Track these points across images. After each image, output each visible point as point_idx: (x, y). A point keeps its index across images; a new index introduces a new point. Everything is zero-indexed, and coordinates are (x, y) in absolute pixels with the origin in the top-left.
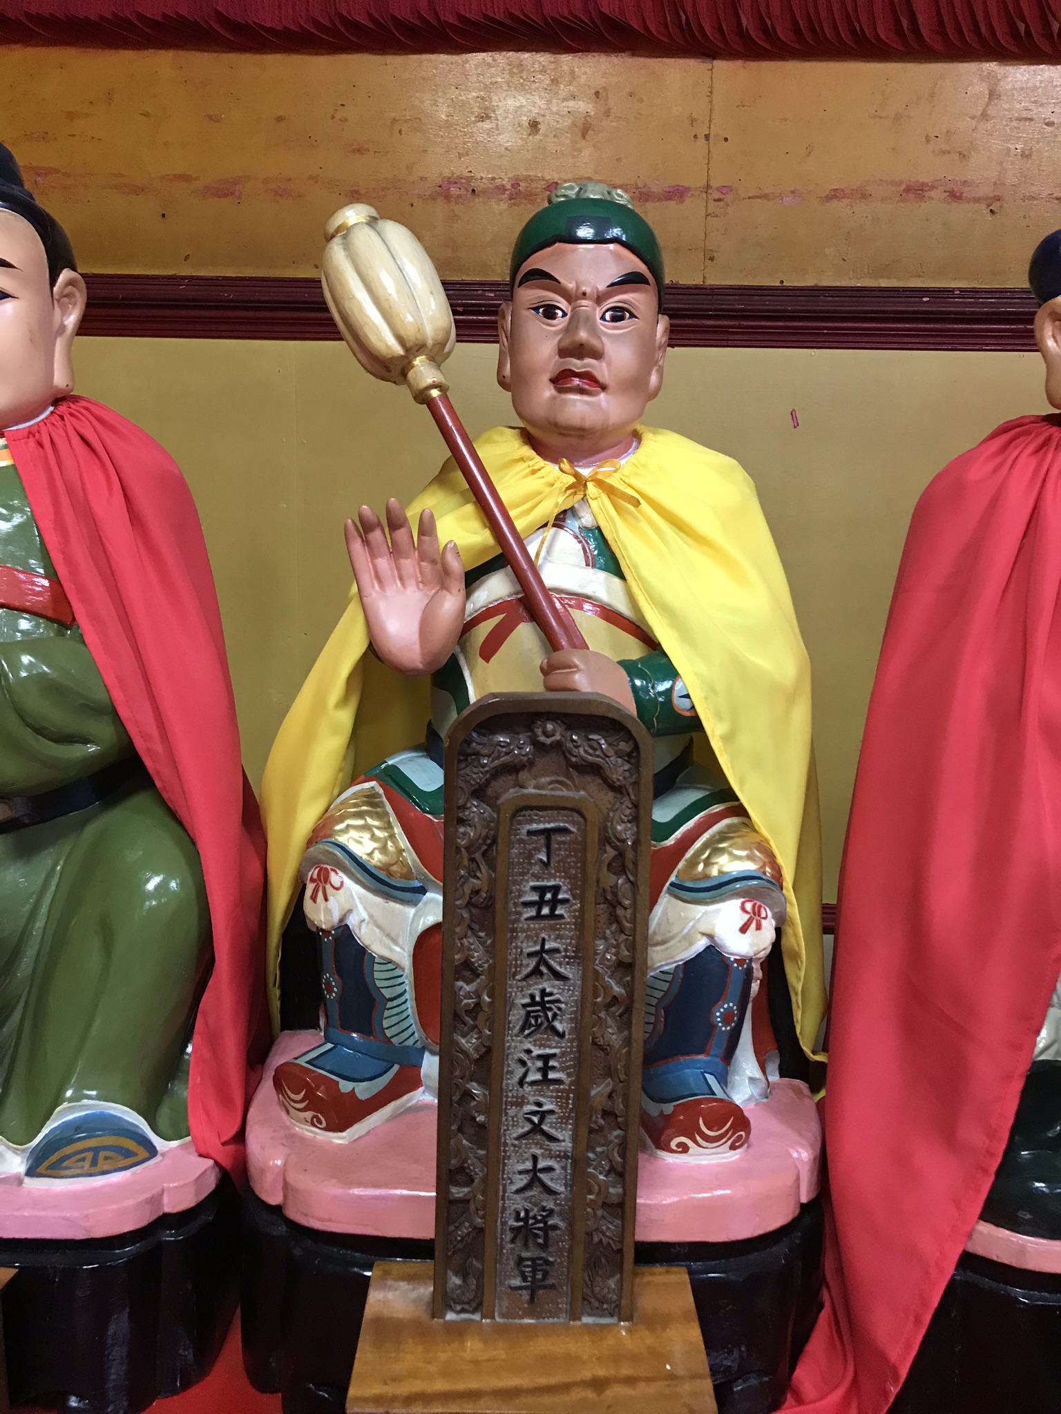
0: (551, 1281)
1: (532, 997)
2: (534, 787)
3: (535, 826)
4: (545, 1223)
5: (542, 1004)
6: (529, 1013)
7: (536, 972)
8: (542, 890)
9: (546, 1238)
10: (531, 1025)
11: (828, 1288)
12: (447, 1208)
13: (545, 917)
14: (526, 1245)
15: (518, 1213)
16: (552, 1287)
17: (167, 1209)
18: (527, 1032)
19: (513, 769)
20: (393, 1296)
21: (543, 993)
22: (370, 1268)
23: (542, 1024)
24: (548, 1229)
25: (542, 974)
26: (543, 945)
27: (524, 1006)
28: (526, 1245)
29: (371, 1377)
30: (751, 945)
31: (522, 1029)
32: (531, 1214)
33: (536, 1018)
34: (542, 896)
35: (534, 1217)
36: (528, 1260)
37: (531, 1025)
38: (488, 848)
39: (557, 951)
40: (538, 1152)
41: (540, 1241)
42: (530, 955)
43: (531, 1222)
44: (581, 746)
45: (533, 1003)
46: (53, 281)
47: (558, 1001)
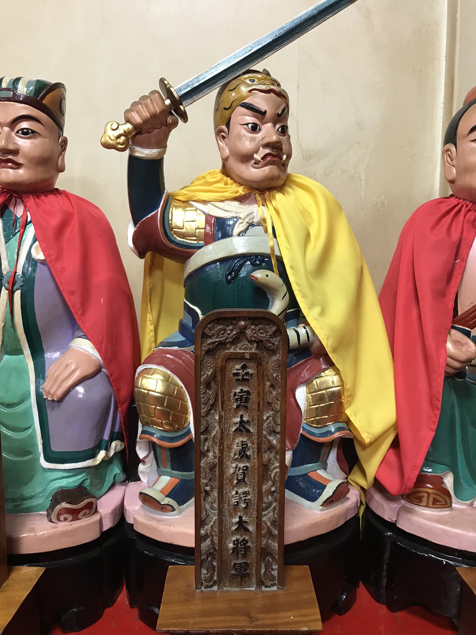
11: (240, 199)
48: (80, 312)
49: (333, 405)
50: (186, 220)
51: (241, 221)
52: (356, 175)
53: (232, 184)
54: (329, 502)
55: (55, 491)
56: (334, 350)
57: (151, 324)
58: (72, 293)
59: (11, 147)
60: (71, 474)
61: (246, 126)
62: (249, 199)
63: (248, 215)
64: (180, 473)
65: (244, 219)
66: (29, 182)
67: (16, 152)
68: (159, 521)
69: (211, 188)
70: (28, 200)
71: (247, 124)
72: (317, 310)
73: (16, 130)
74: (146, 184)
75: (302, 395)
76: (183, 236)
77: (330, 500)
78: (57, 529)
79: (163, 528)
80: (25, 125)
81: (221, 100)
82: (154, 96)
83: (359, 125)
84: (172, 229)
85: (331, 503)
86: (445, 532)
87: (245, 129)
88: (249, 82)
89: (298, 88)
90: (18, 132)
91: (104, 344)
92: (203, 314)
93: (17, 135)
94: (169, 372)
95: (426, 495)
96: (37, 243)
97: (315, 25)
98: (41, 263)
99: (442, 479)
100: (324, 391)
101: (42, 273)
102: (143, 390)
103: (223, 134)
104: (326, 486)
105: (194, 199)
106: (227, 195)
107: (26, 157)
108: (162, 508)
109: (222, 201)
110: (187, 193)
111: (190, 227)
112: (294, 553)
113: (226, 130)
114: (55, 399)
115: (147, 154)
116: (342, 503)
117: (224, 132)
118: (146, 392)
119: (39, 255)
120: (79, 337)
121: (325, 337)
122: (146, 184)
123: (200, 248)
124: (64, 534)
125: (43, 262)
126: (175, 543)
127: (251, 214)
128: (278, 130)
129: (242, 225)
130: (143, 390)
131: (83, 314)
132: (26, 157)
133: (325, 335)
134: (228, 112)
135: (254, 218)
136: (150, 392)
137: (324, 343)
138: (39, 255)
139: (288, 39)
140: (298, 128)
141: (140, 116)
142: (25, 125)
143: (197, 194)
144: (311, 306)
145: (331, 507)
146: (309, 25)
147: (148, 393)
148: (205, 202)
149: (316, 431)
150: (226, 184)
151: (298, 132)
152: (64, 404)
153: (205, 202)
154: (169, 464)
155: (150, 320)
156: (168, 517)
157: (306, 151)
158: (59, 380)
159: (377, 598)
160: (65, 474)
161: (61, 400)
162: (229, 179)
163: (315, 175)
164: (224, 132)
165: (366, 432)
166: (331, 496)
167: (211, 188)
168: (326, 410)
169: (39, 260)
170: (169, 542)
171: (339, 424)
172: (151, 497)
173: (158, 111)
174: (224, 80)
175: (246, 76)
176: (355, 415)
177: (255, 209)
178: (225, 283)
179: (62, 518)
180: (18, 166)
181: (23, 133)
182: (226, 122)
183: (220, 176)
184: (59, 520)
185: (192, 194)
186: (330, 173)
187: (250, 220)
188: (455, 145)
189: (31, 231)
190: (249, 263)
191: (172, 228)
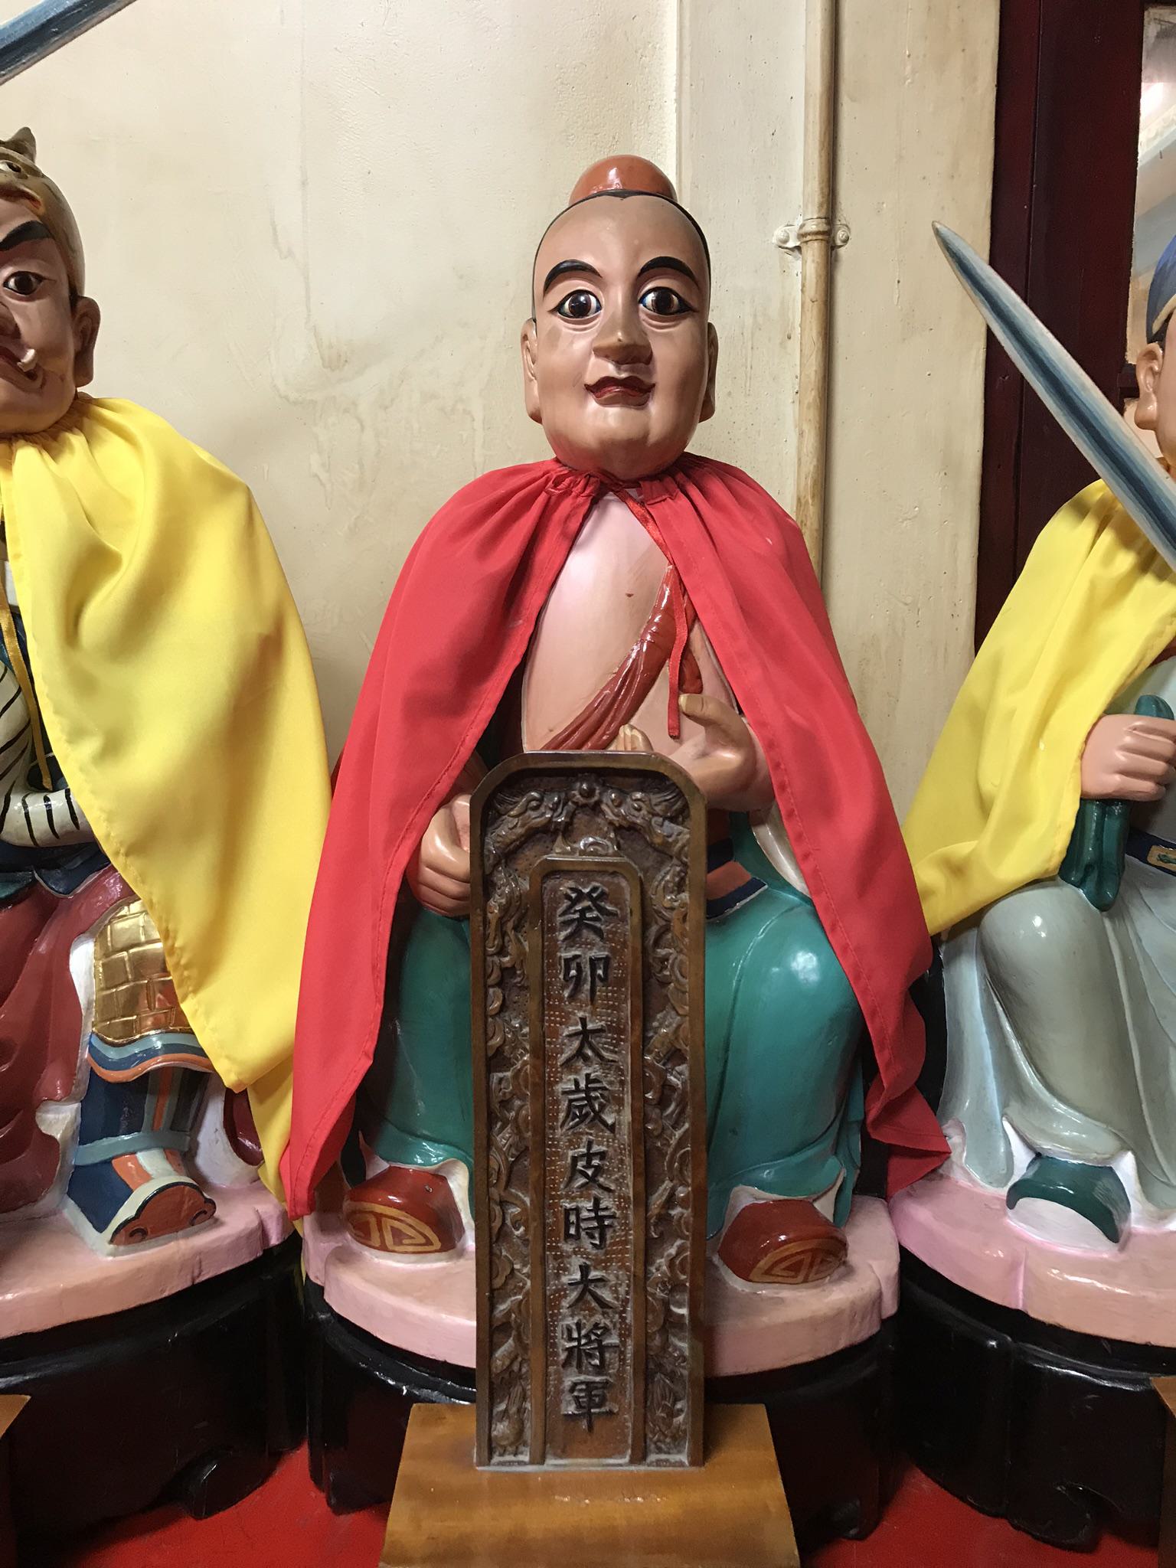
1: (577, 1083)
2: (559, 853)
6: (571, 1101)
7: (579, 1054)
9: (602, 1238)
10: (575, 1116)
12: (490, 1333)
15: (570, 1331)
20: (431, 1435)
23: (587, 1114)
25: (586, 1059)
26: (584, 1025)
28: (579, 1366)
29: (404, 1520)
31: (564, 913)
32: (583, 1332)
35: (587, 1336)
37: (575, 1116)
41: (597, 1362)
43: (583, 1341)
45: (578, 1090)
47: (604, 1089)
49: (149, 987)
52: (460, 407)
54: (135, 1233)
56: (136, 848)
72: (90, 746)
75: (83, 962)
77: (131, 1227)
83: (461, 277)
85: (138, 1236)
86: (400, 1316)
89: (304, 183)
95: (373, 1220)
97: (105, 11)
99: (444, 1179)
100: (125, 954)
104: (131, 1192)
112: (722, 1395)
116: (186, 1237)
121: (104, 816)
128: (6, 284)
133: (101, 810)
137: (99, 832)
139: (34, 49)
140: (307, 289)
144: (76, 735)
145: (141, 1245)
146: (87, 14)
149: (112, 1054)
151: (308, 298)
157: (331, 347)
163: (355, 404)
165: (228, 1057)
166: (133, 1219)
168: (131, 1004)
171: (170, 1036)
176: (208, 1014)
186: (392, 400)
188: (1163, 348)
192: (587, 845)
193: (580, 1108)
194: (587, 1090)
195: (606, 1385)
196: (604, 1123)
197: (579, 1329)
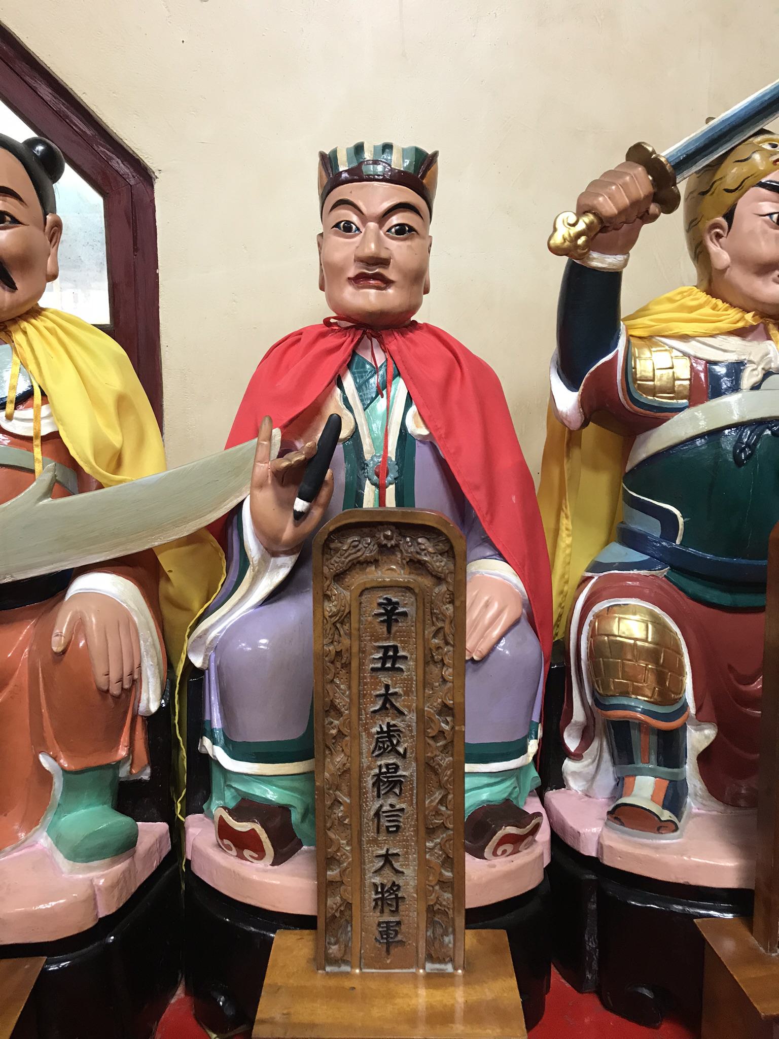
0: (399, 937)
1: (381, 728)
2: (375, 575)
3: (378, 693)
4: (396, 895)
5: (391, 733)
8: (386, 649)
10: (380, 749)
11: (742, 333)
12: (325, 888)
13: (388, 669)
14: (382, 912)
16: (401, 942)
17: (103, 913)
18: (377, 753)
19: (367, 563)
20: (289, 952)
21: (388, 723)
22: (274, 932)
24: (397, 898)
25: (387, 709)
27: (378, 733)
28: (382, 912)
30: (596, 467)
33: (383, 742)
34: (385, 653)
35: (387, 891)
36: (383, 922)
38: (343, 618)
39: (397, 854)
40: (390, 682)
41: (393, 909)
42: (377, 696)
44: (408, 546)
45: (382, 731)
46: (40, 499)
48: (488, 518)
50: (660, 365)
51: (754, 366)
53: (726, 310)
55: (707, 793)
57: (568, 536)
58: (477, 488)
59: (384, 254)
60: (499, 779)
61: (768, 217)
62: (755, 332)
63: (763, 357)
64: (670, 770)
65: (758, 364)
66: (400, 310)
67: (384, 262)
68: (657, 848)
69: (693, 315)
70: (390, 339)
71: (770, 215)
73: (386, 227)
74: (589, 311)
76: (653, 391)
78: (496, 869)
79: (672, 859)
80: (395, 220)
81: (717, 177)
82: (636, 172)
84: (635, 380)
87: (766, 222)
88: (769, 148)
90: (389, 230)
91: (526, 568)
92: (683, 517)
93: (387, 236)
94: (657, 610)
96: (413, 409)
98: (420, 441)
101: (423, 457)
102: (618, 639)
103: (718, 230)
105: (666, 333)
106: (725, 325)
107: (400, 270)
108: (659, 829)
109: (712, 336)
110: (653, 323)
111: (662, 378)
112: (479, 918)
113: (725, 223)
114: (475, 658)
115: (610, 264)
117: (721, 227)
118: (632, 642)
119: (417, 428)
120: (485, 558)
122: (589, 311)
123: (680, 410)
124: (508, 876)
125: (423, 440)
126: (693, 882)
127: (767, 355)
129: (755, 372)
130: (618, 639)
131: (491, 522)
132: (400, 270)
134: (731, 197)
135: (771, 361)
136: (639, 643)
138: (417, 428)
141: (615, 204)
142: (395, 220)
143: (672, 325)
147: (635, 644)
148: (685, 338)
150: (714, 308)
152: (486, 667)
153: (685, 338)
154: (653, 758)
155: (567, 529)
156: (667, 840)
158: (479, 627)
159: (579, 985)
160: (486, 780)
161: (484, 659)
162: (719, 302)
164: (721, 227)
167: (693, 315)
169: (420, 435)
170: (681, 881)
172: (649, 810)
173: (642, 196)
174: (728, 144)
175: (760, 138)
177: (770, 348)
178: (733, 466)
179: (499, 852)
180: (388, 283)
181: (397, 232)
182: (724, 211)
183: (703, 297)
184: (495, 854)
185: (664, 325)
187: (767, 364)
189: (400, 389)
190: (768, 432)
191: (637, 380)
192: (392, 572)
193: (383, 742)
194: (389, 731)
195: (398, 923)
196: (398, 753)
197: (382, 888)
